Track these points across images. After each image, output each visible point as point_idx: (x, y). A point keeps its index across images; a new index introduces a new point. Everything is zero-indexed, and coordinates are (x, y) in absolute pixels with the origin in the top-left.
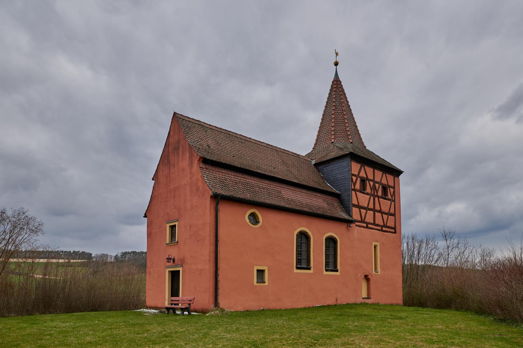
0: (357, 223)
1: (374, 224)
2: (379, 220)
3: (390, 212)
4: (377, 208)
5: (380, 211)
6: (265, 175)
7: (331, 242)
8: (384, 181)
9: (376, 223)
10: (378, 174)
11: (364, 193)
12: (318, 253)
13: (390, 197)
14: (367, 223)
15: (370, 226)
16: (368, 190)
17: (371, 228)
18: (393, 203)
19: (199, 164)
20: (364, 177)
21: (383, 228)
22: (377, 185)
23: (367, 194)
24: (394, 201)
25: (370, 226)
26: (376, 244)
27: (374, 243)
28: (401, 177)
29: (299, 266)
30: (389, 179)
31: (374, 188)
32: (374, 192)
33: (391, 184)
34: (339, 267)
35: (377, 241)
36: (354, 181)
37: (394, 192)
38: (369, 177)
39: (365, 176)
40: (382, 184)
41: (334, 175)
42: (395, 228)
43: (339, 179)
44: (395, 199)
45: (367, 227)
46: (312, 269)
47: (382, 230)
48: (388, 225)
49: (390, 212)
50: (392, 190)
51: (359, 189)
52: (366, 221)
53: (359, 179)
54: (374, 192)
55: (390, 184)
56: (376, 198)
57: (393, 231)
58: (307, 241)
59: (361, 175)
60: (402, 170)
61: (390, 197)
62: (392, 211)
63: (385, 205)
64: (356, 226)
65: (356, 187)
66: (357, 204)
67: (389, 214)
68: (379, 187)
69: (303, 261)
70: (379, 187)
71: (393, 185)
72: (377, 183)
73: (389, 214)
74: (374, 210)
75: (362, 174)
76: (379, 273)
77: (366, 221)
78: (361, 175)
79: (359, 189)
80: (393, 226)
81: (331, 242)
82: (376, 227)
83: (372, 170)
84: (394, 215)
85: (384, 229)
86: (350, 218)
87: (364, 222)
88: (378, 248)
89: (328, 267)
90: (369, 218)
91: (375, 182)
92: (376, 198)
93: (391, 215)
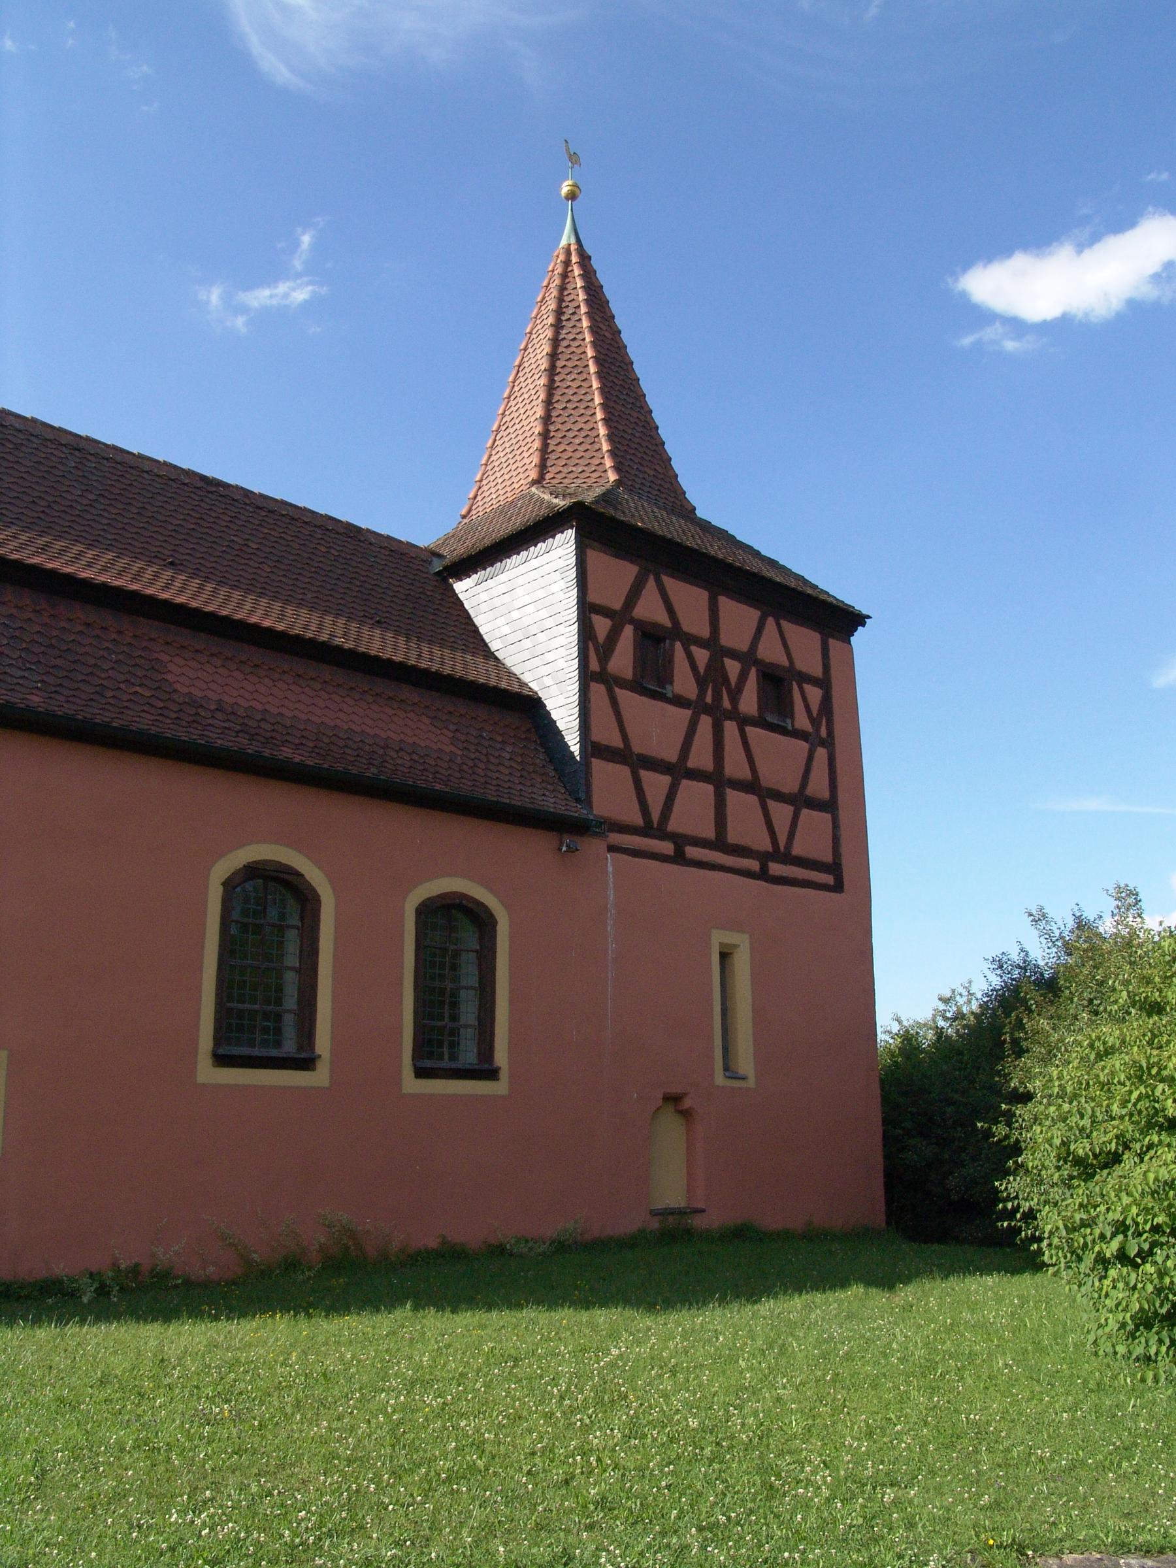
0: (616, 838)
1: (719, 843)
2: (746, 821)
3: (809, 791)
4: (735, 765)
5: (751, 786)
6: (70, 578)
7: (454, 926)
8: (770, 651)
9: (732, 837)
10: (739, 621)
11: (784, 731)
12: (361, 980)
13: (802, 721)
14: (680, 841)
15: (692, 852)
16: (684, 683)
18: (821, 752)
20: (656, 625)
21: (772, 863)
22: (733, 668)
23: (679, 701)
24: (828, 743)
25: (692, 852)
26: (730, 938)
27: (719, 937)
28: (860, 639)
29: (428, 1063)
30: (804, 646)
31: (713, 677)
32: (717, 697)
33: (809, 662)
34: (501, 1057)
35: (735, 926)
37: (827, 700)
39: (664, 619)
40: (757, 662)
41: (515, 615)
42: (835, 868)
43: (534, 629)
44: (830, 733)
45: (679, 858)
46: (504, 1074)
47: (763, 875)
48: (797, 850)
49: (809, 791)
50: (815, 694)
51: (628, 674)
52: (673, 826)
53: (628, 631)
54: (717, 697)
55: (800, 665)
56: (730, 727)
57: (829, 879)
58: (481, 939)
60: (861, 606)
62: (818, 786)
63: (779, 758)
64: (612, 849)
66: (618, 743)
67: (800, 800)
68: (743, 676)
69: (260, 1019)
70: (743, 676)
71: (818, 672)
72: (734, 654)
73: (800, 800)
74: (718, 779)
75: (649, 608)
76: (751, 1083)
77: (673, 826)
79: (628, 674)
80: (828, 857)
81: (454, 926)
83: (818, 636)
84: (829, 806)
85: (775, 868)
86: (577, 811)
87: (661, 833)
88: (742, 963)
89: (430, 1055)
90: (693, 809)
91: (719, 652)
92: (730, 727)
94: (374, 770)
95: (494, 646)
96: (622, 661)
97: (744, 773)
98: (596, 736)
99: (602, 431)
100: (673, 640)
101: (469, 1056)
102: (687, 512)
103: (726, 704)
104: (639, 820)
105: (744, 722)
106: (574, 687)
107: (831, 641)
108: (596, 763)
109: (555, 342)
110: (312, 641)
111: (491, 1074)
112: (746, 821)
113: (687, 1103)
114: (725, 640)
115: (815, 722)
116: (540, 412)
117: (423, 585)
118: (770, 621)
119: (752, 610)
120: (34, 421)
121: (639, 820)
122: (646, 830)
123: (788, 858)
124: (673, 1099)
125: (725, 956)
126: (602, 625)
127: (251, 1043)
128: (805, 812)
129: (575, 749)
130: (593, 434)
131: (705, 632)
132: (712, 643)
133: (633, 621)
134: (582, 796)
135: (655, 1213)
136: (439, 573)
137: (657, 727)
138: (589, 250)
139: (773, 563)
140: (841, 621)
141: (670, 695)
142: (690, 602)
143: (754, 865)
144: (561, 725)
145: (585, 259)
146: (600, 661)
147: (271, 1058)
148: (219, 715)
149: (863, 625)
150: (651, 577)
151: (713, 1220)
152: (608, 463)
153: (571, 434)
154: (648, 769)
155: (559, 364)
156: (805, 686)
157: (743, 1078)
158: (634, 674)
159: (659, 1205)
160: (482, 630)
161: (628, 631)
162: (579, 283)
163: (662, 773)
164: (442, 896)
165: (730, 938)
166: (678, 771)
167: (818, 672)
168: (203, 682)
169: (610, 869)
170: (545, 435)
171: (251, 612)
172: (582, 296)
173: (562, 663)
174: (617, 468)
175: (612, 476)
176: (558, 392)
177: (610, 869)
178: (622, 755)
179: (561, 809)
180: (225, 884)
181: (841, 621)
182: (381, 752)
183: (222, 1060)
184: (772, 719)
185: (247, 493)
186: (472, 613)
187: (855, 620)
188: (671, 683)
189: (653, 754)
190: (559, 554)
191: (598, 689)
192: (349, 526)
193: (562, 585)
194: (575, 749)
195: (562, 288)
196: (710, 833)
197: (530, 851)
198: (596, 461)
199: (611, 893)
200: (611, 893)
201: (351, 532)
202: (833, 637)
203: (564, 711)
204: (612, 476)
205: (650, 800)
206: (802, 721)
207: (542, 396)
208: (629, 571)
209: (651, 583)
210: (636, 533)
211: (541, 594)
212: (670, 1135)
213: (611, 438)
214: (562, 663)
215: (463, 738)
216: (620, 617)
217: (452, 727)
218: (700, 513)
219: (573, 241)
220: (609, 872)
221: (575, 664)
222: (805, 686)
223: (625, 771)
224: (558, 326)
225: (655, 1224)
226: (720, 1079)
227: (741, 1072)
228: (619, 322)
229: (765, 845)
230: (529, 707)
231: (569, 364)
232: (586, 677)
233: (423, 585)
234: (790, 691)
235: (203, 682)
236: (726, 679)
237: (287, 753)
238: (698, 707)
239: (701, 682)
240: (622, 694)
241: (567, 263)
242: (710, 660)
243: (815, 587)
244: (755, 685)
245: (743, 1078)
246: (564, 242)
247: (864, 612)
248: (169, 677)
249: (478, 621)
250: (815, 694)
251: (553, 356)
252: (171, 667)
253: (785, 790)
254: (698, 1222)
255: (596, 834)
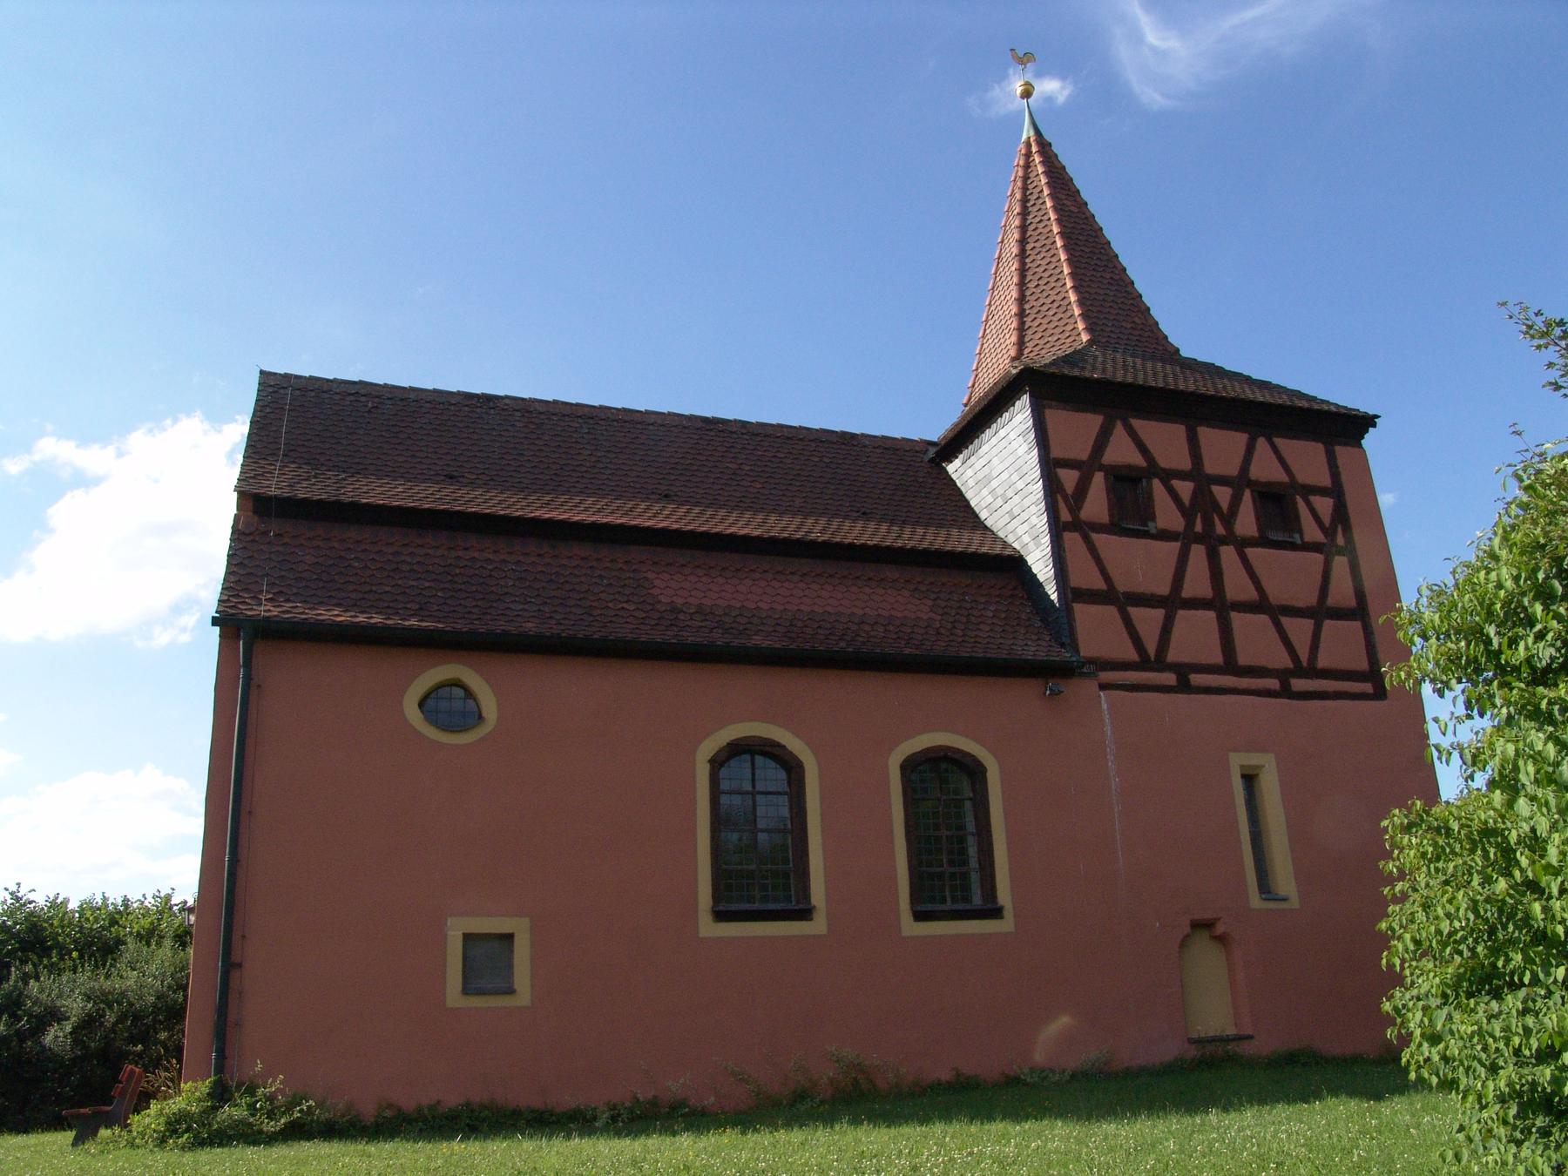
1: (1230, 665)
2: (1256, 640)
3: (1330, 602)
5: (1260, 605)
7: (943, 785)
8: (1265, 468)
9: (1243, 659)
10: (1223, 449)
11: (1293, 547)
12: (855, 837)
15: (1197, 679)
16: (1167, 515)
17: (1208, 690)
19: (87, 1152)
21: (1294, 680)
22: (1223, 494)
23: (1165, 535)
24: (1350, 550)
25: (1197, 679)
26: (1253, 759)
27: (1237, 761)
28: (1370, 441)
30: (1307, 459)
31: (1202, 504)
32: (1208, 523)
34: (1004, 896)
36: (1225, 505)
38: (1163, 463)
39: (1138, 460)
40: (1251, 484)
45: (1184, 687)
47: (1286, 692)
48: (1323, 662)
49: (1330, 602)
51: (1105, 518)
53: (1099, 479)
54: (1208, 523)
55: (1303, 477)
56: (1228, 553)
57: (1368, 687)
58: (973, 784)
59: (1111, 456)
60: (1364, 406)
61: (1312, 533)
62: (1342, 592)
63: (1288, 575)
65: (1307, 539)
66: (1100, 584)
68: (1236, 501)
69: (759, 878)
71: (1326, 481)
72: (1223, 481)
74: (1219, 604)
75: (1120, 451)
76: (1295, 903)
77: (1172, 657)
78: (1111, 456)
79: (1105, 518)
80: (1362, 664)
82: (1244, 682)
84: (1359, 612)
85: (1298, 684)
86: (1066, 655)
87: (1160, 664)
88: (1270, 785)
90: (1195, 636)
92: (1228, 553)
93: (1339, 614)
94: (843, 644)
95: (983, 515)
96: (1096, 505)
97: (1251, 594)
98: (1075, 581)
99: (1073, 297)
100: (1149, 479)
101: (977, 900)
102: (1170, 355)
103: (1220, 529)
104: (1132, 655)
105: (1242, 544)
106: (1046, 540)
107: (1338, 449)
108: (1079, 609)
109: (1023, 228)
110: (975, 555)
111: (995, 913)
112: (1256, 640)
113: (1220, 929)
114: (1210, 468)
115: (1329, 532)
116: (1015, 294)
117: (917, 475)
118: (1261, 443)
119: (1238, 434)
120: (555, 402)
121: (1132, 655)
122: (1144, 663)
123: (1313, 672)
124: (1203, 926)
125: (1250, 779)
126: (1069, 478)
127: (751, 899)
128: (1328, 624)
129: (1054, 597)
130: (1065, 302)
131: (1185, 464)
132: (1196, 474)
133: (1101, 468)
134: (1066, 640)
135: (1192, 1041)
136: (932, 460)
137: (1142, 564)
138: (1048, 137)
139: (1265, 385)
140: (1350, 427)
141: (1153, 531)
142: (1166, 441)
143: (1273, 683)
144: (1041, 578)
145: (1045, 147)
146: (1070, 510)
147: (770, 912)
148: (698, 617)
149: (1374, 425)
150: (1119, 424)
151: (1265, 1045)
152: (1081, 326)
153: (1045, 308)
154: (1136, 605)
155: (1029, 247)
156: (1312, 498)
157: (1284, 899)
158: (1111, 515)
159: (1195, 1036)
160: (973, 504)
161: (1099, 479)
162: (1040, 169)
163: (1153, 607)
164: (928, 750)
165: (1253, 759)
166: (1172, 603)
167: (1326, 481)
168: (685, 590)
169: (1105, 706)
170: (1021, 314)
171: (982, 544)
172: (1044, 180)
173: (1034, 520)
174: (1089, 329)
175: (1085, 337)
176: (1030, 273)
177: (1105, 706)
178: (1107, 596)
179: (1042, 655)
180: (712, 761)
181: (1350, 427)
182: (855, 627)
183: (720, 916)
184: (1275, 536)
185: (744, 424)
186: (963, 489)
187: (1365, 422)
188: (1154, 519)
189: (1141, 590)
190: (1018, 420)
191: (1072, 539)
192: (844, 434)
193: (1025, 447)
194: (1054, 597)
195: (1026, 178)
196: (1217, 658)
197: (1015, 702)
198: (1069, 327)
199: (1108, 730)
200: (1108, 730)
201: (847, 440)
202: (1340, 444)
203: (1041, 564)
204: (1085, 337)
205: (1142, 633)
206: (1312, 533)
207: (1015, 280)
208: (1094, 421)
209: (1119, 429)
210: (1112, 388)
211: (1011, 459)
212: (1207, 964)
213: (1081, 303)
214: (1034, 520)
215: (943, 604)
216: (1085, 469)
217: (933, 596)
218: (1184, 353)
219: (1032, 133)
220: (1103, 711)
221: (1045, 518)
222: (1312, 498)
223: (1112, 611)
224: (1024, 213)
225: (1193, 1052)
226: (1255, 901)
227: (1282, 892)
228: (1085, 195)
229: (1285, 662)
230: (1014, 565)
231: (1038, 245)
232: (1057, 529)
233: (917, 475)
234: (1295, 503)
235: (685, 590)
236: (1215, 505)
237: (757, 640)
238: (1186, 539)
239: (1187, 513)
240: (1099, 539)
241: (1028, 154)
242: (1194, 492)
243: (1314, 399)
244: (1251, 505)
245: (1284, 899)
246: (1024, 137)
247: (1371, 413)
248: (655, 592)
249: (968, 495)
250: (1324, 505)
251: (1023, 242)
252: (657, 582)
253: (1300, 604)
254: (1246, 1049)
255: (1083, 675)
